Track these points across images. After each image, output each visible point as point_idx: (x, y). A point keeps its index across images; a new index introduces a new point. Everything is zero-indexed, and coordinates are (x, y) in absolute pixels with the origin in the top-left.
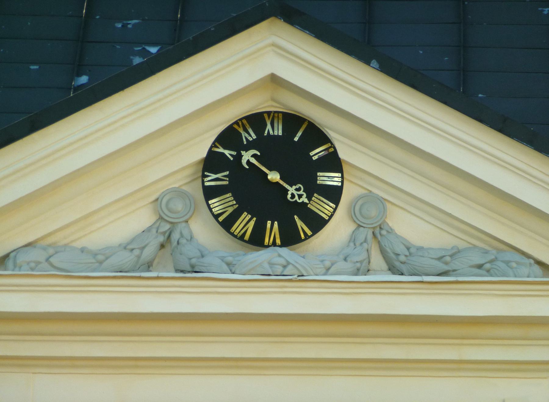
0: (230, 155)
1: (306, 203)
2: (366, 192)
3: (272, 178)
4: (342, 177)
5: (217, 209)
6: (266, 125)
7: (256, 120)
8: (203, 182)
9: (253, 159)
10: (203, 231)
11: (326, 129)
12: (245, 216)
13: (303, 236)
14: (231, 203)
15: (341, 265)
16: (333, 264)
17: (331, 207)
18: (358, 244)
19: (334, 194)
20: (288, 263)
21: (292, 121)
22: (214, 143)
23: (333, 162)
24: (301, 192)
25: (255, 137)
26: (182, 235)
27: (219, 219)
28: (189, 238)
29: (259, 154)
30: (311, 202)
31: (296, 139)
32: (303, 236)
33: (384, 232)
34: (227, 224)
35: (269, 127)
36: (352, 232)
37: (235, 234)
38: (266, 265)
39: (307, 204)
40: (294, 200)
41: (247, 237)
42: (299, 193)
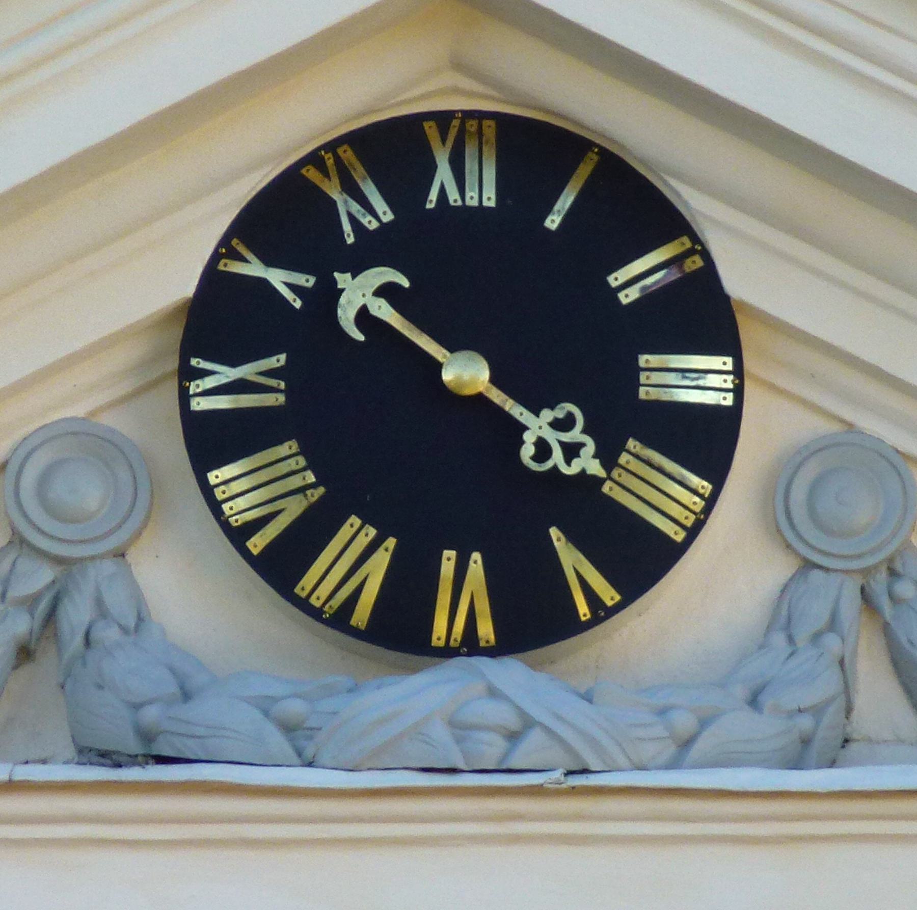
0: (291, 287)
1: (594, 477)
2: (835, 427)
3: (458, 379)
4: (738, 371)
5: (241, 503)
6: (432, 168)
7: (392, 148)
8: (184, 397)
9: (382, 302)
10: (186, 592)
11: (674, 183)
12: (354, 533)
13: (583, 609)
14: (295, 482)
15: (739, 725)
16: (704, 723)
17: (695, 492)
18: (802, 635)
19: (706, 441)
20: (529, 723)
21: (536, 148)
22: (225, 241)
23: (701, 314)
24: (575, 435)
25: (388, 216)
26: (102, 610)
27: (250, 544)
28: (131, 623)
29: (406, 283)
30: (615, 474)
31: (553, 222)
32: (583, 609)
33: (905, 589)
34: (281, 566)
35: (444, 174)
36: (778, 589)
37: (315, 602)
38: (441, 733)
39: (600, 481)
40: (549, 464)
41: (361, 616)
42: (567, 437)
